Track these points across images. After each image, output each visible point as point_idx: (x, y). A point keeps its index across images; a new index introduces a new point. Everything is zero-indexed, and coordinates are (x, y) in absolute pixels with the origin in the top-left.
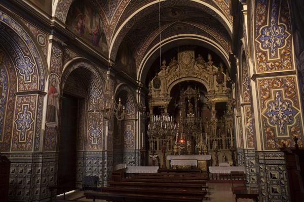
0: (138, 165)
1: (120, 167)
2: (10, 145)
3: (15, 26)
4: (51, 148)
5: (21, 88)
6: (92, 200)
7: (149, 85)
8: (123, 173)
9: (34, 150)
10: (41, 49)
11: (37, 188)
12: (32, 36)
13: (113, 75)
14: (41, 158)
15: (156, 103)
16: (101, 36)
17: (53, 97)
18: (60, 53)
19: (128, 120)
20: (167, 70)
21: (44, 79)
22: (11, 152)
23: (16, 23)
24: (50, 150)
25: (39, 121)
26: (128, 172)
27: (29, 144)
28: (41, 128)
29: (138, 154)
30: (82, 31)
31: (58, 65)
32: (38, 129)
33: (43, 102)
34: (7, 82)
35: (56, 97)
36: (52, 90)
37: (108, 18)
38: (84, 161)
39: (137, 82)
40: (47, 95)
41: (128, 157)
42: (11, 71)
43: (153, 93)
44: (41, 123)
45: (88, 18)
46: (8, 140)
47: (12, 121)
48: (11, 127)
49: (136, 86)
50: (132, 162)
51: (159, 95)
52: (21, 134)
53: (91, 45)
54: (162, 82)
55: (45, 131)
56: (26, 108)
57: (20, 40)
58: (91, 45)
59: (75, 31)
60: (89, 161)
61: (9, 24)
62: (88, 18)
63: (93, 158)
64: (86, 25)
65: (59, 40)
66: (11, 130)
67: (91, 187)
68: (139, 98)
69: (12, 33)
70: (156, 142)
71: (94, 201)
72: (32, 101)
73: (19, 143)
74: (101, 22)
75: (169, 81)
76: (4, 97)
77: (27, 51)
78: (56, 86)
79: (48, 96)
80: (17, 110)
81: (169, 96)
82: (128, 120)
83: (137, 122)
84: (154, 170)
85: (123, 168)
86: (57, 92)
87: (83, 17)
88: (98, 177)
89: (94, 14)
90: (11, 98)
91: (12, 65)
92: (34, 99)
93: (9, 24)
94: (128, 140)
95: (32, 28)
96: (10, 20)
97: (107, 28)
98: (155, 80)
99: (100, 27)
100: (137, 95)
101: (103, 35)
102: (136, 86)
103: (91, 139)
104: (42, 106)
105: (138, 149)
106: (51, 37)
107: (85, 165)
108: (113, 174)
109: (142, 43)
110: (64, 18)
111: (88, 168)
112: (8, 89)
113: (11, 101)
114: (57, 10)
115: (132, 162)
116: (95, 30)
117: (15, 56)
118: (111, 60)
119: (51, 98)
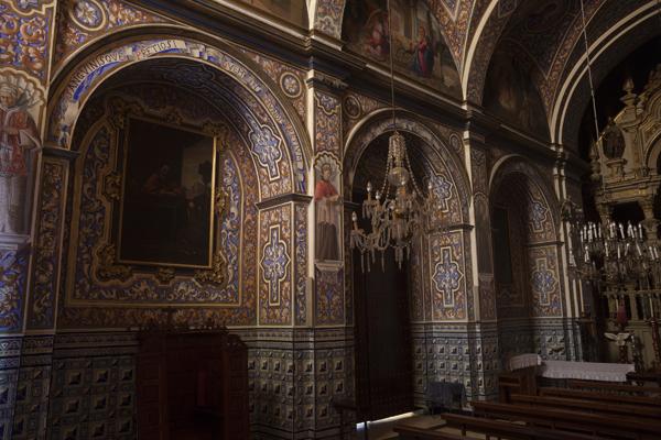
0: (577, 359)
1: (522, 361)
2: (255, 311)
3: (231, 67)
4: (333, 317)
5: (265, 193)
6: (484, 436)
7: (593, 153)
8: (535, 376)
9: (296, 324)
10: (291, 105)
11: (308, 403)
12: (268, 80)
13: (482, 140)
14: (312, 339)
15: (618, 197)
16: (436, 52)
17: (328, 204)
18: (335, 105)
19: (537, 245)
20: (639, 105)
21: (304, 168)
22: (258, 326)
23: (233, 61)
24: (331, 322)
25: (300, 260)
26: (549, 374)
27: (285, 311)
28: (306, 273)
29: (574, 330)
30: (386, 49)
31: (334, 132)
32: (299, 278)
33: (306, 218)
34: (239, 185)
35: (335, 203)
36: (325, 189)
37: (450, 6)
38: (429, 347)
39: (553, 148)
40: (313, 201)
41: (548, 338)
42: (243, 162)
43: (605, 172)
44: (306, 263)
45: (395, 15)
46: (251, 301)
47: (255, 264)
48: (255, 275)
49: (549, 159)
50: (557, 351)
51: (624, 174)
52: (272, 290)
53: (412, 75)
54: (627, 136)
55: (315, 282)
56: (275, 235)
57: (246, 93)
58: (412, 75)
59: (368, 51)
60: (439, 347)
61: (219, 65)
62: (395, 15)
63: (447, 338)
64: (394, 33)
65: (328, 77)
66: (255, 281)
67: (447, 403)
68: (561, 189)
69: (227, 82)
70: (627, 299)
71: (488, 438)
72: (285, 218)
73: (270, 307)
74: (434, 19)
75: (650, 133)
76: (236, 214)
77: (263, 115)
78: (334, 179)
79: (316, 204)
80: (262, 239)
81: (654, 173)
82: (537, 245)
83: (563, 248)
84: (615, 373)
85: (532, 364)
86: (336, 193)
87: (382, 18)
88: (463, 385)
89: (412, 4)
90: (249, 217)
91: (245, 148)
92: (288, 211)
93: (219, 65)
94: (543, 294)
95: (267, 64)
96: (221, 56)
97: (449, 29)
98: (607, 136)
99: (431, 32)
100: (557, 182)
101: (443, 49)
102: (549, 159)
103: (439, 295)
104: (306, 225)
105: (573, 318)
106: (311, 74)
107: (431, 356)
108: (501, 379)
109: (553, 48)
110: (336, 27)
111: (440, 363)
112: (240, 198)
113: (249, 222)
114: (317, 14)
115: (557, 351)
116: (419, 40)
117: (246, 129)
118: (469, 103)
119: (323, 206)
